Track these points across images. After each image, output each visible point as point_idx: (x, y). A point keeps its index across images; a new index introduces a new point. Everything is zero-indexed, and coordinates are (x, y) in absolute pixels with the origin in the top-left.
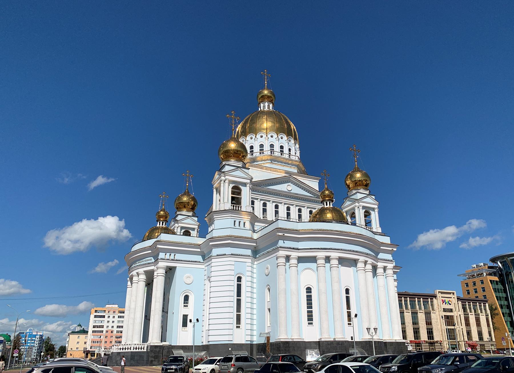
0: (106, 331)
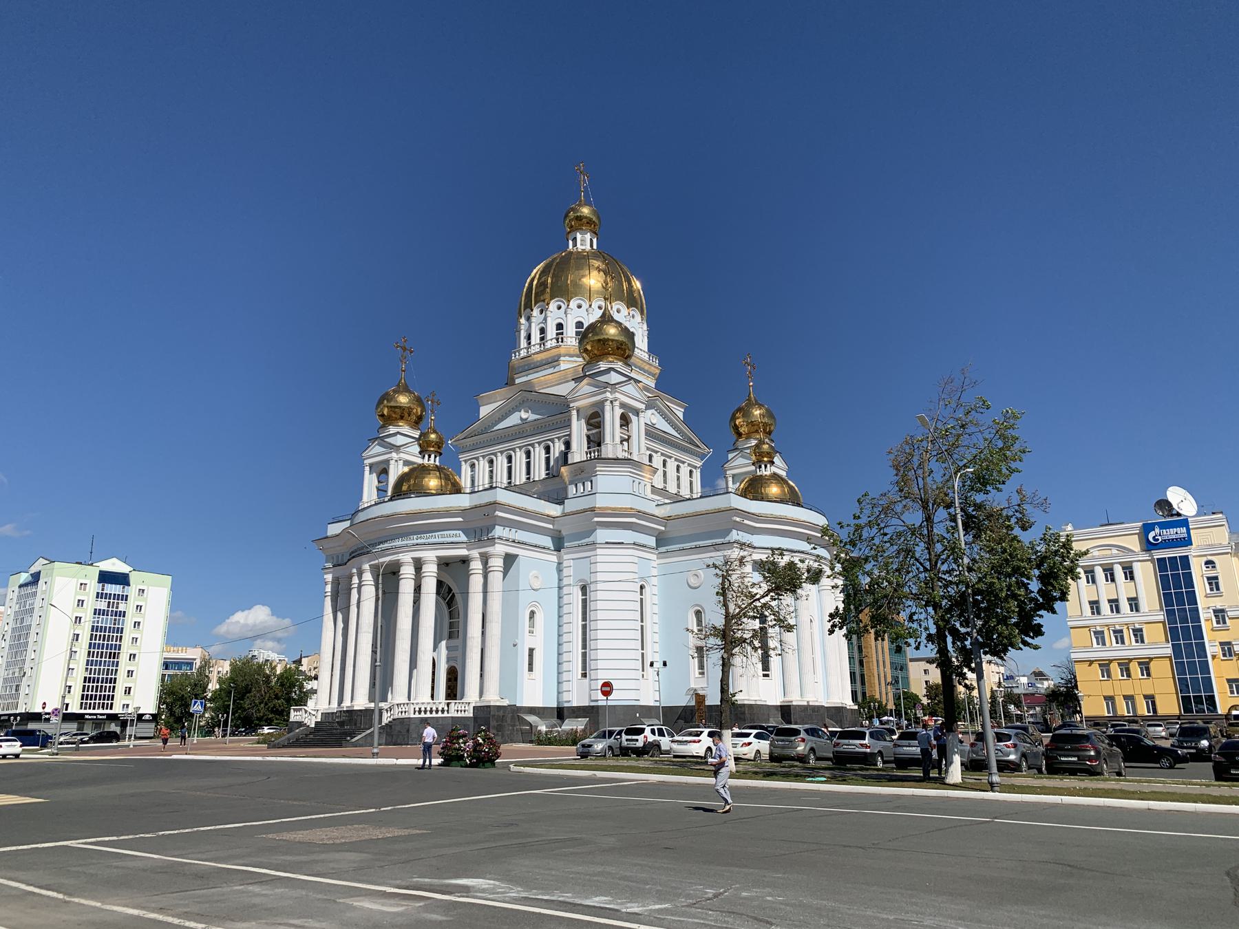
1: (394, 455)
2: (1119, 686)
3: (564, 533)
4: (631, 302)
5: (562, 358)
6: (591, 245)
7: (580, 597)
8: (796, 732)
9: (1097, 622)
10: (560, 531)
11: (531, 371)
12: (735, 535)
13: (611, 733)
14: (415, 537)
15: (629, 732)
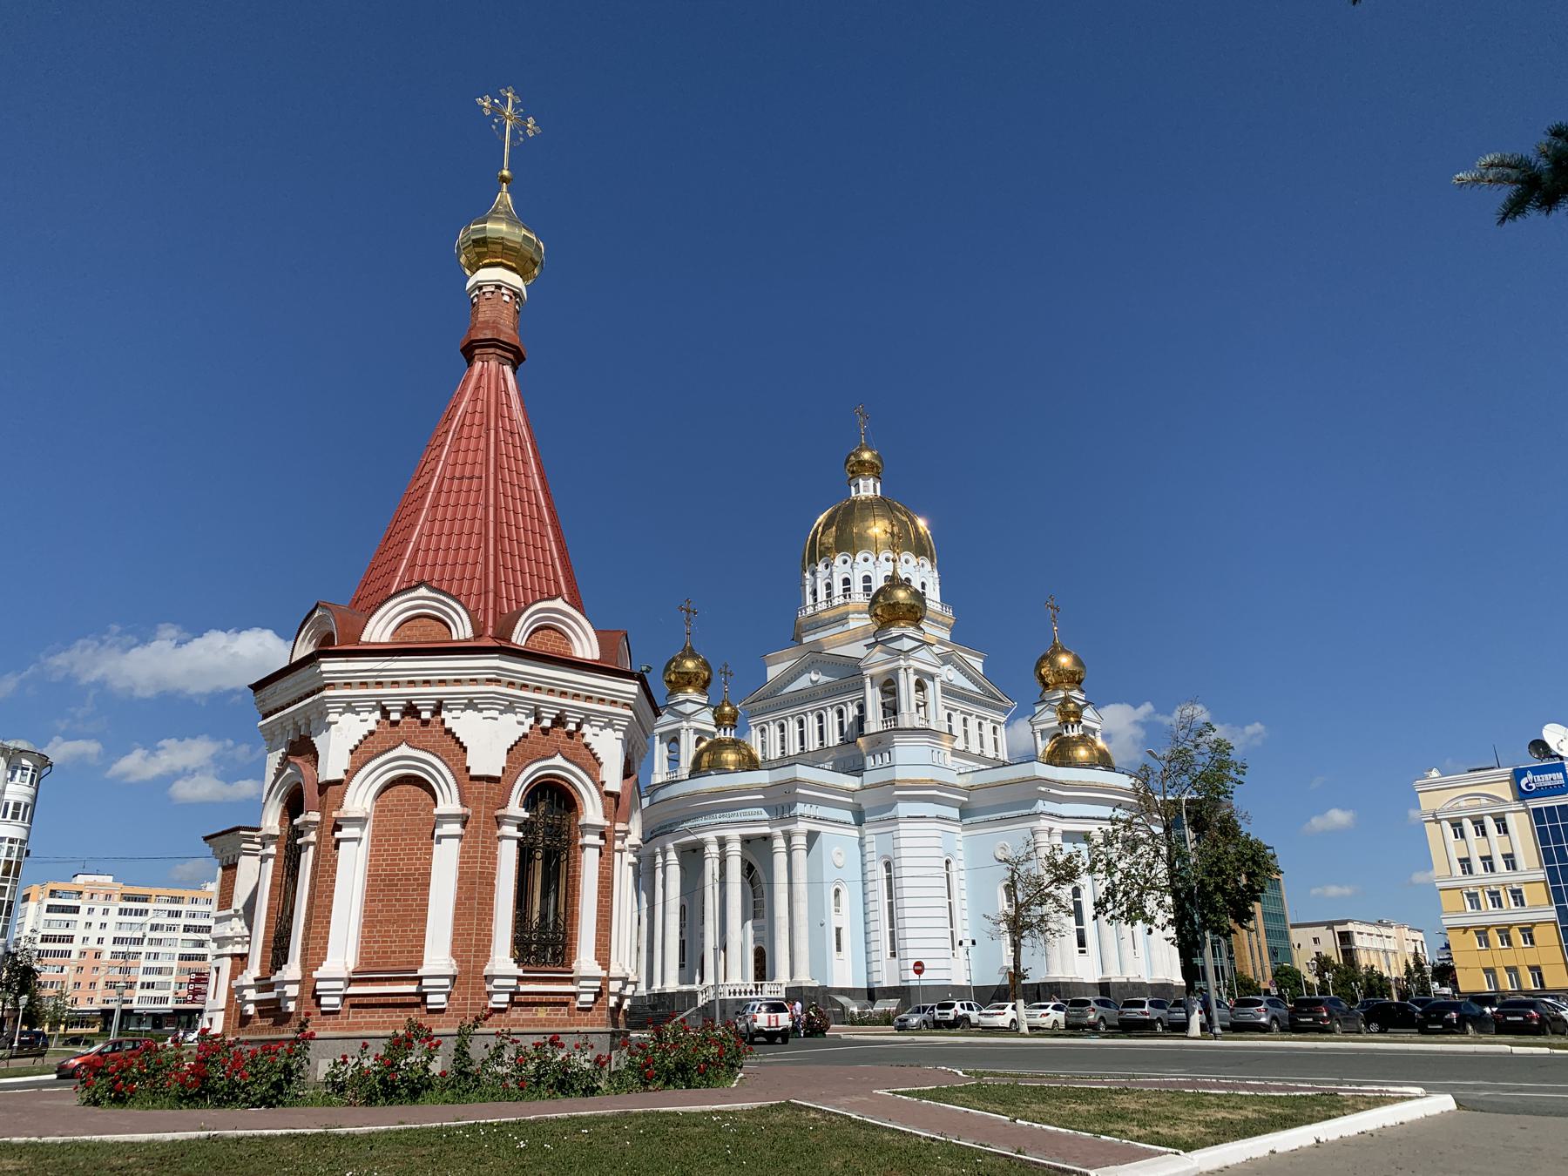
0: (81, 953)
1: (684, 724)
2: (1500, 956)
3: (864, 807)
4: (920, 549)
5: (851, 616)
6: (875, 491)
7: (885, 874)
8: (1087, 1003)
9: (1469, 882)
10: (860, 805)
11: (820, 629)
12: (1041, 806)
13: (925, 1009)
14: (718, 815)
15: (941, 1007)
